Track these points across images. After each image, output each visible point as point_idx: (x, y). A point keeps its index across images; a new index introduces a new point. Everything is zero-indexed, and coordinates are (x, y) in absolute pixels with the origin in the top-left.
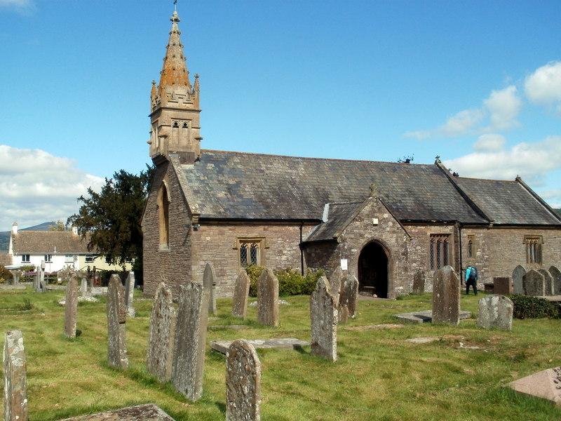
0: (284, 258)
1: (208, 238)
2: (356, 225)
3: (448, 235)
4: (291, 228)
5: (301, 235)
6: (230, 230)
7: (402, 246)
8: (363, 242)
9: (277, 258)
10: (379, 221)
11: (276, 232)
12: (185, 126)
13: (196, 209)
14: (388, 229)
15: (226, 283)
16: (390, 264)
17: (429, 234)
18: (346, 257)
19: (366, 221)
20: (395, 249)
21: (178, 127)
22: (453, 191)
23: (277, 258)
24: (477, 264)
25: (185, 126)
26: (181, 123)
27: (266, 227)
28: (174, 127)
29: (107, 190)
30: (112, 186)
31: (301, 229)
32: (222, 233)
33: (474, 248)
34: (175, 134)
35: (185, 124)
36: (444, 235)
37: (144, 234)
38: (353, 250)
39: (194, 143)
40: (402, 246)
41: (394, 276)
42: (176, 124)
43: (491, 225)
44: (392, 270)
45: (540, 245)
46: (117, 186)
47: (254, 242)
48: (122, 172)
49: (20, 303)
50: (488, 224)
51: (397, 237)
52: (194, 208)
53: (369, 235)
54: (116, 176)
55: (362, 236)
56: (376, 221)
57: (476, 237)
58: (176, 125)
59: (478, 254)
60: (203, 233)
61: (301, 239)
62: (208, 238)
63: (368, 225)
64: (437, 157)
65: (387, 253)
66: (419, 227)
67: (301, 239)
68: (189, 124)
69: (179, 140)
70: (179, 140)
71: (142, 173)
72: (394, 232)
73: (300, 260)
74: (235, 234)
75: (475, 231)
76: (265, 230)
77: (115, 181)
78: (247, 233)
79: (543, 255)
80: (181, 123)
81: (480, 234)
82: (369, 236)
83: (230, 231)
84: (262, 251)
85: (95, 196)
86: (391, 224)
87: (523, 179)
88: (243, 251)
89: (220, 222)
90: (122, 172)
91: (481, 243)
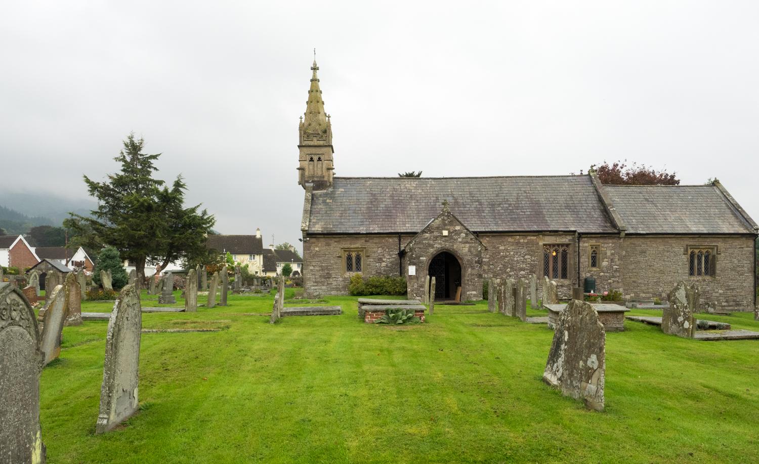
0: (384, 264)
1: (317, 249)
2: (426, 237)
3: (567, 245)
4: (391, 240)
5: (400, 245)
6: (335, 242)
7: (477, 255)
9: (377, 265)
10: (449, 232)
11: (376, 243)
12: (319, 159)
14: (460, 240)
15: (332, 284)
16: (462, 270)
17: (541, 243)
18: (414, 264)
19: (436, 234)
20: (469, 258)
21: (313, 161)
23: (377, 265)
24: (602, 274)
25: (319, 159)
26: (315, 158)
27: (368, 239)
28: (310, 161)
32: (328, 245)
33: (599, 259)
34: (311, 167)
35: (319, 158)
36: (562, 245)
38: (421, 258)
39: (325, 173)
40: (477, 255)
41: (466, 282)
42: (312, 158)
43: (623, 234)
44: (465, 276)
45: (714, 257)
47: (358, 251)
50: (619, 233)
51: (470, 247)
53: (438, 245)
55: (432, 246)
56: (445, 233)
57: (602, 247)
58: (312, 160)
59: (605, 263)
60: (313, 244)
61: (400, 249)
62: (317, 249)
63: (437, 237)
65: (459, 261)
66: (529, 238)
67: (400, 249)
68: (322, 158)
69: (314, 172)
70: (314, 172)
72: (467, 242)
73: (399, 266)
74: (340, 246)
75: (601, 241)
76: (366, 241)
78: (350, 244)
79: (718, 267)
80: (315, 158)
81: (608, 247)
82: (439, 246)
83: (336, 243)
86: (463, 235)
87: (724, 183)
88: (349, 258)
91: (609, 253)
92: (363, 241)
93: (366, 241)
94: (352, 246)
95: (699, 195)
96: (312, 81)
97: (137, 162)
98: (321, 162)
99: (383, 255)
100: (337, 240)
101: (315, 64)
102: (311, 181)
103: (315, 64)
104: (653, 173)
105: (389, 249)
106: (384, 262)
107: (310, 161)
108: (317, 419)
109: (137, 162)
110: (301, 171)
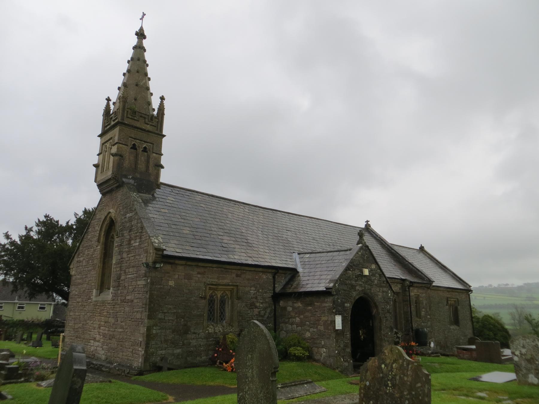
5: (274, 284)
6: (199, 273)
8: (355, 295)
11: (248, 280)
13: (160, 243)
22: (387, 257)
29: (26, 239)
30: (32, 234)
31: (274, 277)
37: (73, 278)
46: (39, 233)
48: (46, 216)
49: (214, 280)
52: (157, 241)
54: (40, 223)
55: (353, 287)
61: (274, 290)
64: (367, 221)
67: (274, 290)
71: (68, 223)
76: (237, 276)
77: (35, 229)
83: (199, 276)
84: (232, 303)
85: (13, 243)
89: (189, 263)
90: (46, 216)
92: (234, 275)
93: (237, 276)
94: (221, 281)
95: (177, 234)
96: (134, 48)
97: (85, 209)
98: (146, 154)
99: (256, 298)
100: (201, 270)
101: (141, 29)
102: (130, 177)
103: (141, 29)
104: (57, 222)
105: (262, 289)
106: (256, 307)
107: (131, 148)
108: (123, 274)
109: (85, 209)
110: (117, 158)
